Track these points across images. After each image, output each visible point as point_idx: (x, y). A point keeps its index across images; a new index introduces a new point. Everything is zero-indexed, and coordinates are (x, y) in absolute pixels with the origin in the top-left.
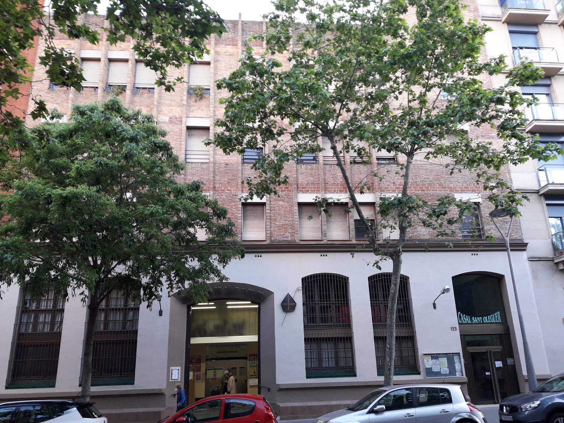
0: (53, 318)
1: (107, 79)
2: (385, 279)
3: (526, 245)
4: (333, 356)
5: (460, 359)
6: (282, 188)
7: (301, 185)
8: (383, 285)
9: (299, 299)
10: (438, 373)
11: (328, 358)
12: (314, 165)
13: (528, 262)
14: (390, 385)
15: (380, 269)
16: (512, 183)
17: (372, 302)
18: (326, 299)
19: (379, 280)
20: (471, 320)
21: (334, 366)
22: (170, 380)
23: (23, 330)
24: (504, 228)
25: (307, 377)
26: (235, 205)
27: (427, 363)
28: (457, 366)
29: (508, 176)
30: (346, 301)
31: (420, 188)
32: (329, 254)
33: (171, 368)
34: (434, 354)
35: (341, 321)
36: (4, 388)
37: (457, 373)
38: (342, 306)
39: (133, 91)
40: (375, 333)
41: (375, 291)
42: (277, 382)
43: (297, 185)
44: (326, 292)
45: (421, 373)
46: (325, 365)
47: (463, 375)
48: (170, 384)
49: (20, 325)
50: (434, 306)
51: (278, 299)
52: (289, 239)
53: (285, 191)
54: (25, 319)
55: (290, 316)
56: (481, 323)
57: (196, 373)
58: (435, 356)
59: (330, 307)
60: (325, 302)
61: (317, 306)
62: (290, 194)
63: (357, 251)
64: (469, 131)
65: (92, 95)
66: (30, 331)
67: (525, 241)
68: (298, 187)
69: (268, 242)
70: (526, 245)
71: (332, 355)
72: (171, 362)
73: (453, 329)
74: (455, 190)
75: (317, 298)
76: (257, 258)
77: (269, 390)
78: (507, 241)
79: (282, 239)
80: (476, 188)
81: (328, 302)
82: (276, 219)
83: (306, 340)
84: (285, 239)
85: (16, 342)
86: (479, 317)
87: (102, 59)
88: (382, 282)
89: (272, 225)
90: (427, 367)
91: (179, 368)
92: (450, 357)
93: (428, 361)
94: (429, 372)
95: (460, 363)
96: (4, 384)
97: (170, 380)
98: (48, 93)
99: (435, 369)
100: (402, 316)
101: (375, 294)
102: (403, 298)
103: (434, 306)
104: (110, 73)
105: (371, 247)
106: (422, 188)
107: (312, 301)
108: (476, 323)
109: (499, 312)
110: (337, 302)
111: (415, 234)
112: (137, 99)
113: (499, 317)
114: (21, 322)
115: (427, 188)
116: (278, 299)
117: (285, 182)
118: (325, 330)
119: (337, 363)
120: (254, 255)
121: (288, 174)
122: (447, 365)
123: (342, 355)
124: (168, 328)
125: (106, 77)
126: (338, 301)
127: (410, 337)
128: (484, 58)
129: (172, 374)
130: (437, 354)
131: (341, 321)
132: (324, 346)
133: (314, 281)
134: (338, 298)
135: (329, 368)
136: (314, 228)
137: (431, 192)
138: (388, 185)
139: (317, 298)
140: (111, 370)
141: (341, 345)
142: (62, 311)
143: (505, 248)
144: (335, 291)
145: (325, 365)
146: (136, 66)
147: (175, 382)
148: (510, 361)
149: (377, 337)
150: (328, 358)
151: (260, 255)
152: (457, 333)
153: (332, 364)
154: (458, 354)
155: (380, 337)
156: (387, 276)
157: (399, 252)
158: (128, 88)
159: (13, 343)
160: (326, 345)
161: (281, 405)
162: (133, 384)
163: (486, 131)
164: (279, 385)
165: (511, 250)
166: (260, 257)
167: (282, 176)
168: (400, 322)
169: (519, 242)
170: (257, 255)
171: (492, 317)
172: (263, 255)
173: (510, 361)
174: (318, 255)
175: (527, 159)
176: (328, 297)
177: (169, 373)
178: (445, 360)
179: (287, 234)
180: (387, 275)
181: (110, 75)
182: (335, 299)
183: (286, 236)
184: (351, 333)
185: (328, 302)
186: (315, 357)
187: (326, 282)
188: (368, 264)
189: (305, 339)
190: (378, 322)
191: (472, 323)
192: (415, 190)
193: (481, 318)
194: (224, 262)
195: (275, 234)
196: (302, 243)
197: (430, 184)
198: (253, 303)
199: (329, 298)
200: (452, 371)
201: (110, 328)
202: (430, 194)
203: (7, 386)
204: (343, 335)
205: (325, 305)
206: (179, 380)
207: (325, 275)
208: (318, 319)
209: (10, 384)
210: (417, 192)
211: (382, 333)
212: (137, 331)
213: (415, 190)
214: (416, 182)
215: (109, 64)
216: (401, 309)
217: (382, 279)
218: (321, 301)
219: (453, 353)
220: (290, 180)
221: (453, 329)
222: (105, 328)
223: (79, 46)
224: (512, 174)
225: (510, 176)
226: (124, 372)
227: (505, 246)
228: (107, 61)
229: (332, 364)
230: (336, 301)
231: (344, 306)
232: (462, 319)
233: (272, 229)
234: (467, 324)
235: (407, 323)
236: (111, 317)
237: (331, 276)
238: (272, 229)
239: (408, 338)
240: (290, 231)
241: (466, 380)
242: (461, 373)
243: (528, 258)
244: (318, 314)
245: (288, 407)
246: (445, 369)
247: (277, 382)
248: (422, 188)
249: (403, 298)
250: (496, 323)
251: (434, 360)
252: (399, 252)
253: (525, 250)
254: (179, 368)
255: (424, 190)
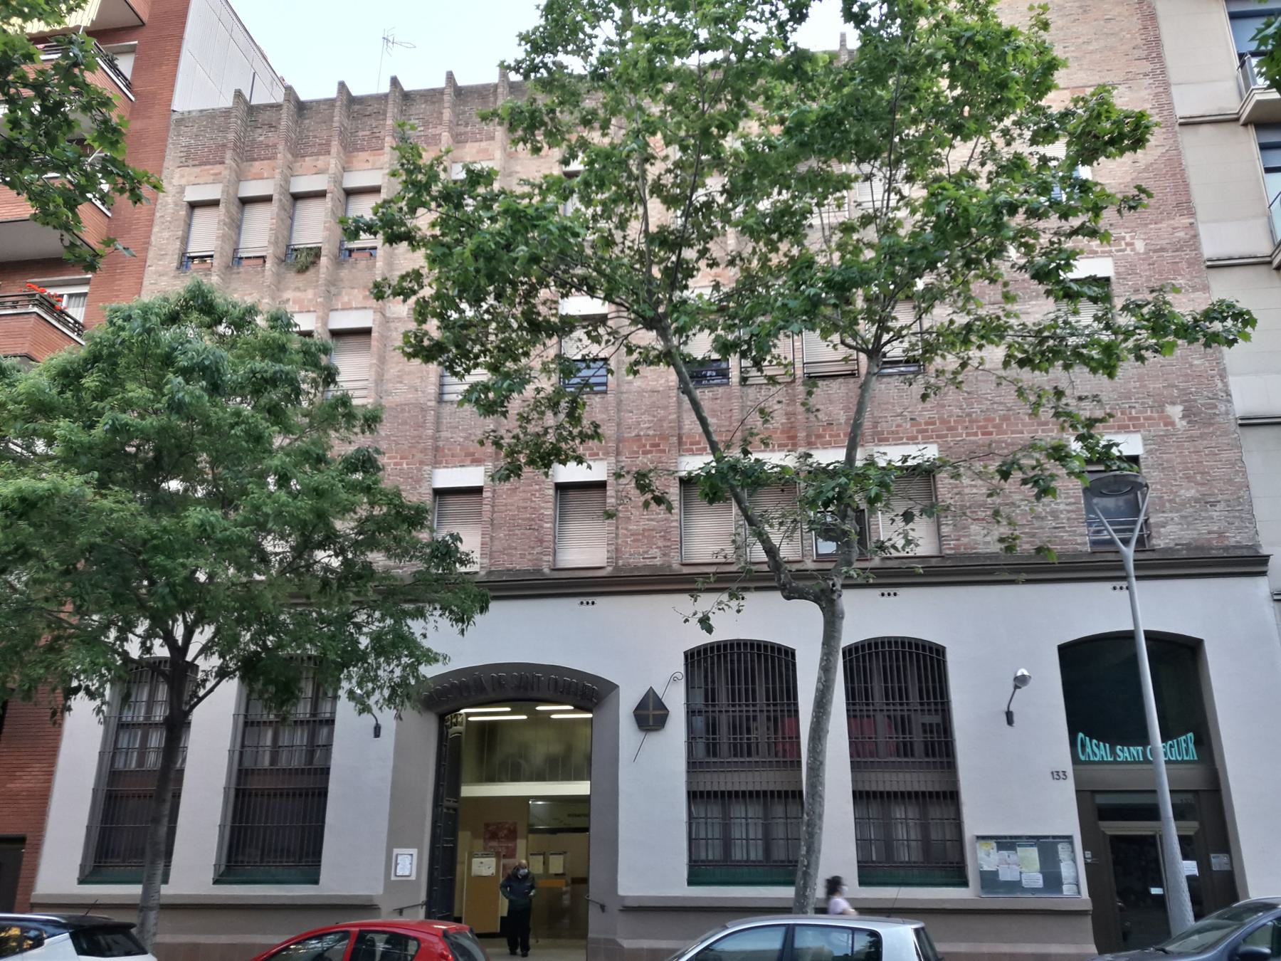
0: (312, 736)
1: (290, 237)
2: (890, 653)
3: (1264, 560)
4: (717, 836)
5: (1073, 851)
6: (645, 446)
7: (689, 436)
8: (885, 668)
9: (676, 701)
10: (1015, 886)
11: (747, 839)
12: (721, 390)
13: (1272, 604)
14: (806, 913)
15: (709, 629)
16: (1229, 401)
17: (851, 707)
18: (901, 698)
19: (877, 653)
20: (1113, 753)
21: (760, 857)
22: (393, 878)
23: (120, 765)
24: (1205, 518)
25: (690, 883)
26: (540, 490)
27: (983, 859)
28: (1066, 870)
29: (1220, 385)
30: (943, 704)
31: (978, 428)
32: (902, 592)
33: (396, 851)
34: (1005, 837)
35: (780, 754)
36: (76, 881)
37: (1065, 888)
38: (783, 717)
39: (336, 258)
40: (854, 781)
41: (866, 682)
42: (621, 892)
43: (680, 437)
44: (899, 681)
45: (971, 883)
46: (738, 854)
47: (1079, 893)
48: (395, 886)
49: (114, 754)
50: (1010, 717)
51: (628, 701)
52: (658, 562)
53: (650, 452)
54: (123, 743)
55: (654, 739)
56: (1139, 762)
57: (503, 861)
58: (1006, 843)
59: (755, 718)
60: (744, 708)
61: (724, 717)
62: (664, 459)
63: (700, 591)
64: (1113, 279)
65: (258, 273)
66: (133, 765)
67: (1264, 551)
68: (680, 442)
69: (608, 571)
70: (1264, 560)
71: (756, 832)
72: (396, 838)
73: (1058, 775)
74: (1134, 426)
75: (723, 699)
76: (585, 607)
77: (603, 908)
78: (1126, 557)
79: (641, 562)
80: (1131, 419)
81: (751, 709)
82: (629, 518)
83: (693, 796)
84: (648, 562)
85: (233, 785)
86: (1133, 745)
87: (275, 198)
88: (884, 660)
89: (621, 531)
90: (986, 868)
91: (414, 851)
92: (1047, 846)
93: (988, 855)
94: (990, 881)
95: (1074, 860)
96: (76, 874)
97: (393, 878)
98: (175, 277)
99: (1006, 875)
100: (939, 743)
101: (866, 689)
102: (935, 698)
103: (1010, 717)
104: (296, 223)
105: (772, 579)
106: (986, 427)
107: (867, 704)
108: (1126, 762)
109: (1191, 735)
110: (772, 708)
111: (964, 540)
112: (344, 273)
113: (1191, 746)
114: (116, 748)
115: (998, 427)
116: (628, 701)
117: (596, 435)
118: (743, 775)
119: (767, 850)
120: (577, 601)
121: (599, 417)
122: (1037, 866)
123: (779, 832)
124: (390, 763)
125: (286, 233)
126: (775, 705)
127: (793, 792)
128: (1161, 90)
129: (397, 864)
130: (1011, 837)
131: (780, 754)
132: (738, 810)
133: (870, 655)
134: (775, 699)
135: (748, 863)
136: (720, 535)
137: (1008, 437)
138: (898, 426)
139: (723, 699)
140: (282, 850)
141: (778, 810)
142: (331, 722)
143: (1123, 574)
144: (767, 683)
145: (738, 854)
146: (347, 204)
147: (404, 883)
148: (1218, 862)
149: (861, 793)
150: (747, 839)
151: (590, 600)
152: (1068, 790)
153: (756, 854)
154: (1069, 839)
155: (874, 793)
156: (903, 646)
157: (833, 592)
158: (323, 252)
159: (95, 791)
160: (743, 809)
161: (627, 944)
162: (316, 882)
163: (1160, 273)
164: (624, 898)
165: (1138, 578)
166: (590, 606)
167: (585, 422)
168: (927, 755)
169: (1245, 553)
170: (585, 600)
171: (1171, 746)
172: (598, 600)
173: (1218, 862)
174: (575, 601)
175: (1173, 345)
176: (903, 694)
177: (390, 862)
178: (1032, 854)
179: (655, 551)
180: (910, 644)
181: (295, 228)
182: (768, 699)
183: (652, 557)
184: (955, 782)
185: (751, 709)
186: (717, 836)
187: (897, 659)
188: (686, 621)
189: (854, 793)
190: (872, 756)
191: (1115, 762)
192: (968, 435)
193: (1140, 748)
194: (463, 622)
195: (627, 551)
196: (686, 570)
197: (1005, 418)
198: (579, 708)
199: (754, 699)
200: (1053, 881)
201: (283, 763)
202: (1005, 442)
203: (87, 872)
204: (771, 787)
205: (744, 714)
206: (413, 877)
207: (739, 645)
208: (725, 748)
209: (92, 873)
210: (972, 438)
211: (722, 784)
212: (328, 769)
213: (968, 435)
214: (969, 415)
215: (294, 206)
216: (938, 725)
217: (884, 653)
218: (734, 706)
219: (1054, 837)
220: (608, 430)
221: (1058, 775)
222: (272, 764)
223: (234, 175)
224: (1232, 380)
225: (1226, 385)
226: (307, 856)
227: (1122, 567)
228: (287, 201)
229: (756, 854)
230: (768, 705)
231: (789, 716)
232: (1089, 750)
233: (620, 541)
234: (1102, 762)
235: (945, 760)
236: (285, 739)
237: (766, 647)
238: (620, 541)
239: (945, 797)
240: (660, 544)
241: (1089, 907)
242: (1074, 887)
243: (1273, 594)
244: (724, 736)
245: (642, 949)
246: (1034, 878)
247: (621, 892)
248: (986, 427)
249: (928, 698)
250: (1183, 762)
251: (1005, 853)
252: (833, 592)
253: (1263, 574)
254: (414, 851)
255: (991, 434)
